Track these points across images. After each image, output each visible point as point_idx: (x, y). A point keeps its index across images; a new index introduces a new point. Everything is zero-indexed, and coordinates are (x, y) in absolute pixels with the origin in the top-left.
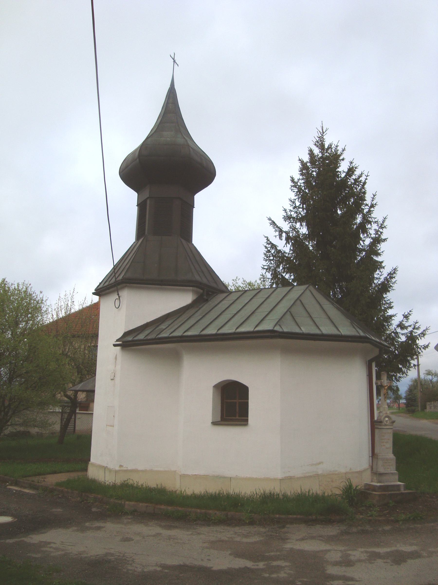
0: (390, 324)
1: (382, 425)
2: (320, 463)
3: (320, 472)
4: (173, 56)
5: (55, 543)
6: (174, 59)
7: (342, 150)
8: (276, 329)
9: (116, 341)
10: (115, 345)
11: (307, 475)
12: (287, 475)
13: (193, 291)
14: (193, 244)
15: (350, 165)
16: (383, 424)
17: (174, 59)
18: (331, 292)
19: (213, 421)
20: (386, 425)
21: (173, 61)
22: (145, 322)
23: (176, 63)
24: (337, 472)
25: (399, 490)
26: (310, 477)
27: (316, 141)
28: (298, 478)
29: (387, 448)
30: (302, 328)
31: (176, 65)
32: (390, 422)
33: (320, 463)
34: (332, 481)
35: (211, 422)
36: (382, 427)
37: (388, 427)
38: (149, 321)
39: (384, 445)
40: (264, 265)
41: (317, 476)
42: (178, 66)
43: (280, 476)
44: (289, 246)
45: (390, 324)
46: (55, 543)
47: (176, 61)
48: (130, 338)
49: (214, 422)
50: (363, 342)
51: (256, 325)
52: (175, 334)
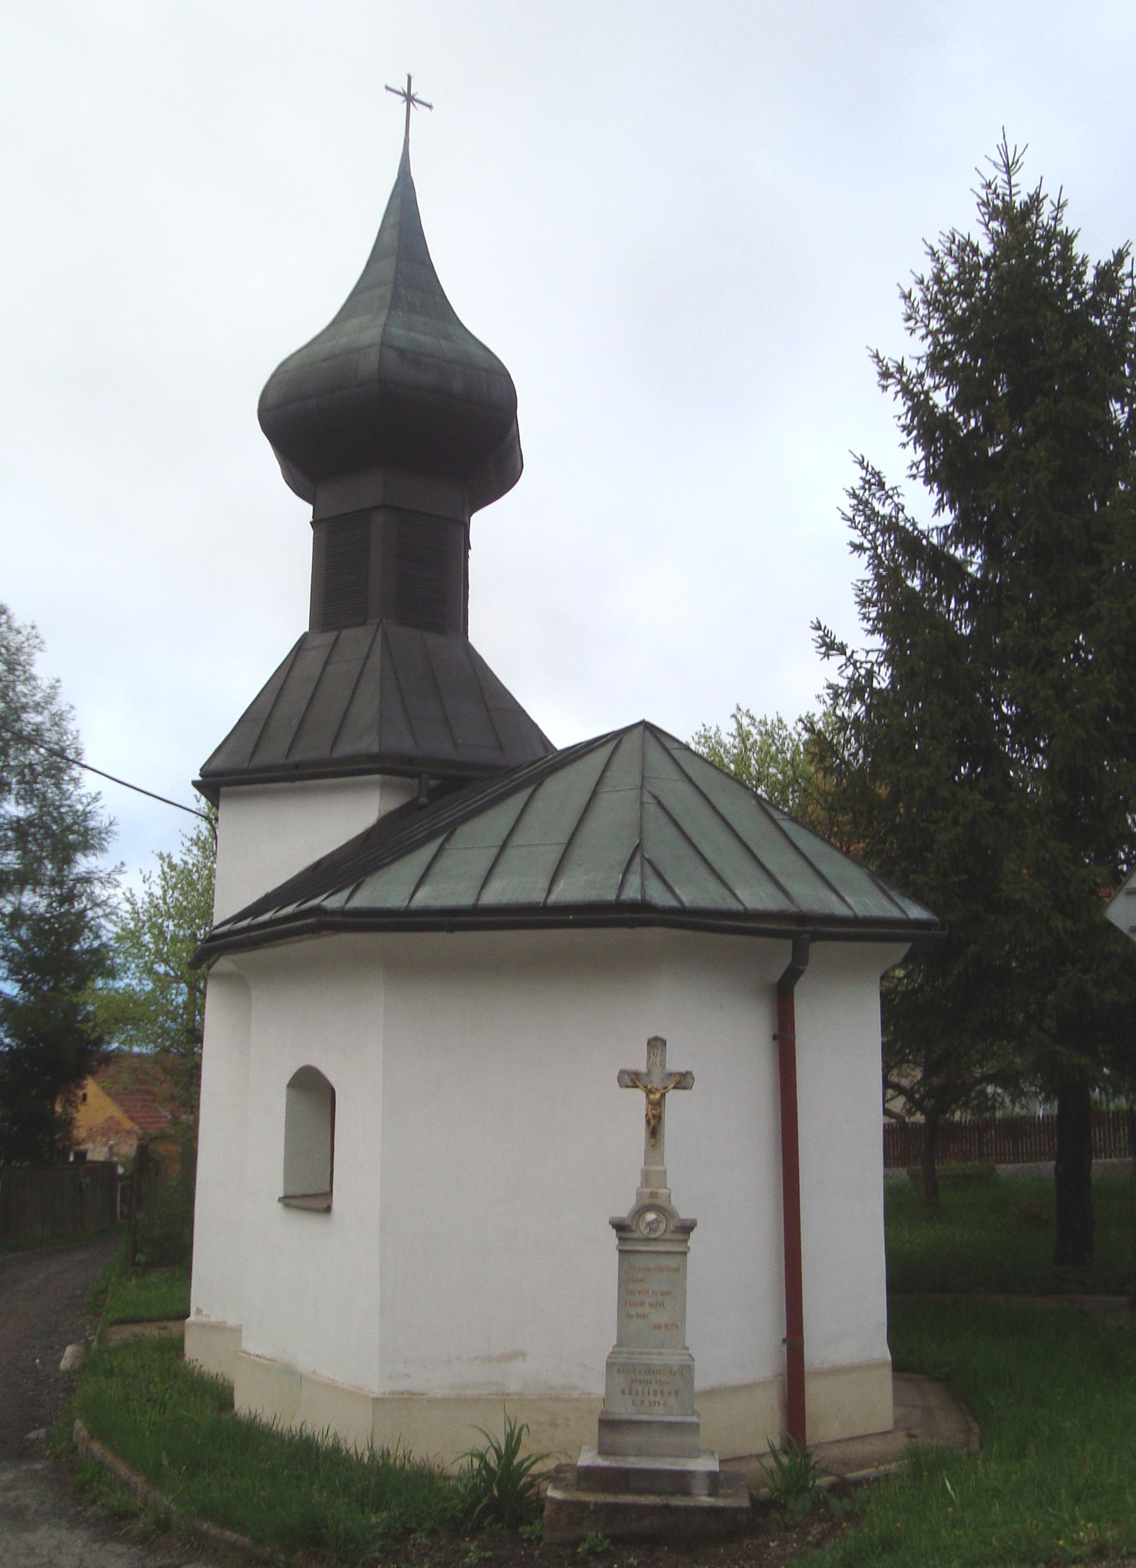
1: (631, 1239)
2: (513, 1356)
3: (514, 1387)
5: (542, 1457)
7: (1053, 208)
11: (469, 1392)
12: (400, 1385)
13: (383, 786)
16: (637, 1235)
19: (297, 1191)
20: (648, 1240)
22: (261, 894)
24: (575, 1394)
25: (686, 1492)
26: (476, 1401)
27: (980, 201)
28: (430, 1400)
29: (657, 1327)
32: (672, 1228)
33: (513, 1356)
34: (554, 1424)
35: (280, 1200)
36: (631, 1248)
37: (661, 1247)
38: (270, 890)
39: (644, 1316)
40: (868, 649)
41: (503, 1398)
43: (376, 1386)
46: (542, 1457)
49: (293, 1197)
50: (633, 924)
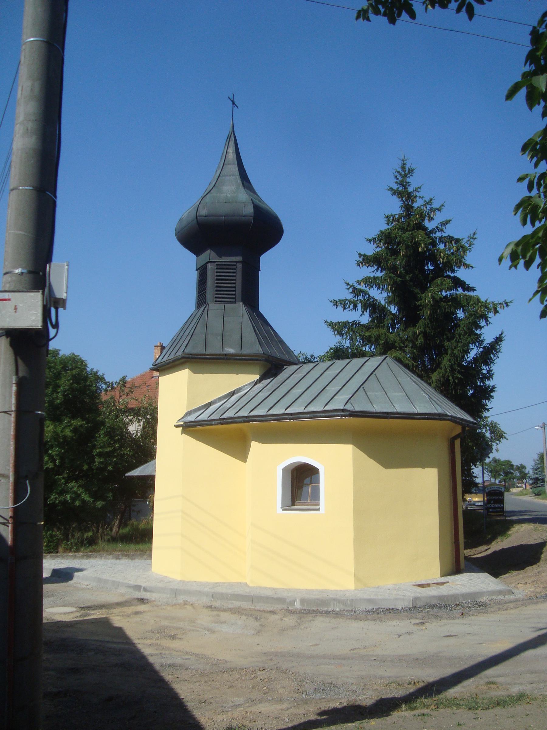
0: (86, 374)
4: (231, 98)
6: (233, 101)
8: (346, 407)
9: (177, 421)
10: (177, 426)
14: (260, 311)
15: (396, 180)
17: (233, 101)
18: (462, 377)
21: (232, 103)
23: (231, 100)
30: (374, 406)
31: (235, 108)
42: (238, 108)
44: (367, 314)
45: (86, 374)
47: (235, 103)
48: (191, 418)
51: (345, 403)
52: (240, 414)
